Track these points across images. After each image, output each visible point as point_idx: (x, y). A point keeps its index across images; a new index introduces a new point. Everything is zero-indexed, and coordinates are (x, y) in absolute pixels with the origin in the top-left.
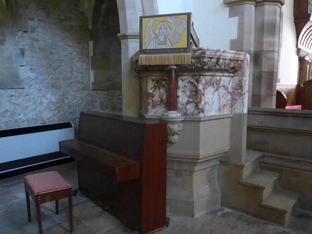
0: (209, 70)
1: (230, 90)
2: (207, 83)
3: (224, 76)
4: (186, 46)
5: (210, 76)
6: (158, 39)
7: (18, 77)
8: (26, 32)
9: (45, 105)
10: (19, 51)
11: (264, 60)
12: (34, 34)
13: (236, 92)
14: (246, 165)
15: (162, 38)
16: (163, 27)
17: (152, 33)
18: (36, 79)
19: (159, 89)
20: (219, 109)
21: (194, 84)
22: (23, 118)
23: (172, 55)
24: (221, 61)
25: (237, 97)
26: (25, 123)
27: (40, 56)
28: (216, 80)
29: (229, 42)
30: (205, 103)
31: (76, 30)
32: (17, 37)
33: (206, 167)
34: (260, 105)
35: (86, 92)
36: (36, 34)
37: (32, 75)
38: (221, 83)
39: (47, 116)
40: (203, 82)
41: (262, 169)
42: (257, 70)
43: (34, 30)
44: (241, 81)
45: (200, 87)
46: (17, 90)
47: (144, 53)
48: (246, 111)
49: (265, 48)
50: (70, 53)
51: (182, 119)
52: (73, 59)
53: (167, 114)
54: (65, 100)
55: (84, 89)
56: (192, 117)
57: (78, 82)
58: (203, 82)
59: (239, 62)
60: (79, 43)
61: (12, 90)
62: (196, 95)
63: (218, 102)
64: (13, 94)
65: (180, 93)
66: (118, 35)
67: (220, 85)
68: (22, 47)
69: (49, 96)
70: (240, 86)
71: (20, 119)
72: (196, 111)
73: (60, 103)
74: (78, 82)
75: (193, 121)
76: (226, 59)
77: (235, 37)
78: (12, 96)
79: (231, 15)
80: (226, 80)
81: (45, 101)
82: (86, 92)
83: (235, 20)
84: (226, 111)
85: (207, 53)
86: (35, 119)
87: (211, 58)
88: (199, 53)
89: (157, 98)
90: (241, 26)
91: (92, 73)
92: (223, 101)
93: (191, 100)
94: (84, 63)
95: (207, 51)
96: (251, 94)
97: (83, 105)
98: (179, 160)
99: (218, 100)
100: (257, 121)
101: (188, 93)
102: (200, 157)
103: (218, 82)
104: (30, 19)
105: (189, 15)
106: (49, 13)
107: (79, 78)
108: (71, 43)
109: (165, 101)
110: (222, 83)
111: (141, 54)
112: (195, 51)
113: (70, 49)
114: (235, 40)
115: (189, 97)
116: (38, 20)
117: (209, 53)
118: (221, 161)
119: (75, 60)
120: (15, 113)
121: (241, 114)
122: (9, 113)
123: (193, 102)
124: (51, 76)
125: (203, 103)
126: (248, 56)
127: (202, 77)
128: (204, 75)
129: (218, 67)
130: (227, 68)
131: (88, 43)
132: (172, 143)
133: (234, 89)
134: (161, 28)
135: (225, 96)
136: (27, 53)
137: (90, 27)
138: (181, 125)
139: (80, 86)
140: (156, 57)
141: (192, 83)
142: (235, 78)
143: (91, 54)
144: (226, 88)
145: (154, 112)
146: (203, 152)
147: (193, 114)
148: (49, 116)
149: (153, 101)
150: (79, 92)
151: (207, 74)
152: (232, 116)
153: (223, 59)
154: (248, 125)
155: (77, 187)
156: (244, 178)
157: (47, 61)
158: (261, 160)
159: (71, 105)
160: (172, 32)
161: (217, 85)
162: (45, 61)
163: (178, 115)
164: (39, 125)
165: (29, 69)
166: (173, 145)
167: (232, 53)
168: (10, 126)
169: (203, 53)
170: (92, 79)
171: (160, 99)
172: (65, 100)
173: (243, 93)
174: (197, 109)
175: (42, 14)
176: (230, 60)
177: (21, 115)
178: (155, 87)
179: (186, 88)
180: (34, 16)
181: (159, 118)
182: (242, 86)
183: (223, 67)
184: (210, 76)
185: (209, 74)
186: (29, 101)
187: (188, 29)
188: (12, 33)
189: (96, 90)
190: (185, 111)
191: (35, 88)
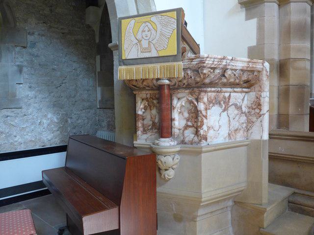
0: (212, 84)
1: (244, 109)
2: (210, 102)
3: (235, 92)
4: (176, 53)
5: (214, 92)
6: (141, 45)
7: (14, 95)
8: (24, 47)
9: (45, 125)
10: (15, 68)
11: (291, 70)
12: (34, 50)
13: (253, 112)
14: (268, 209)
15: (145, 44)
16: (146, 29)
17: (133, 38)
18: (36, 98)
19: (151, 110)
20: (229, 134)
21: (193, 103)
22: (20, 140)
23: (158, 66)
24: (229, 72)
25: (254, 119)
26: (22, 146)
27: (40, 73)
28: (224, 98)
29: (247, 49)
30: (209, 128)
31: (81, 44)
32: (14, 53)
33: (214, 209)
34: (287, 127)
35: (93, 111)
36: (37, 49)
37: (31, 94)
38: (231, 101)
39: (48, 137)
40: (205, 100)
41: (292, 210)
42: (283, 83)
43: (34, 45)
44: (258, 98)
45: (201, 106)
46: (13, 110)
47: (125, 64)
48: (266, 137)
49: (292, 56)
50: (74, 69)
51: (178, 149)
52: (78, 76)
53: (158, 142)
54: (69, 120)
55: (90, 108)
56: (191, 146)
57: (83, 100)
58: (205, 100)
59: (256, 73)
60: (86, 58)
61: (9, 110)
62: (195, 118)
63: (227, 125)
64: (9, 114)
65: (175, 115)
66: (110, 45)
67: (230, 104)
68: (20, 64)
69: (50, 116)
70: (258, 105)
71: (16, 141)
72: (196, 139)
73: (63, 123)
74: (83, 100)
75: (192, 150)
76: (236, 70)
77: (253, 43)
78: (7, 117)
79: (248, 18)
80: (238, 97)
81: (45, 121)
82: (93, 111)
83: (254, 22)
84: (240, 137)
85: (207, 62)
86: (33, 141)
87: (214, 69)
88: (196, 62)
89: (148, 122)
90: (260, 29)
91: (99, 89)
92: (235, 124)
93: (190, 124)
94: (91, 79)
95: (208, 59)
96: (275, 113)
97: (89, 125)
98: (262, 149)
99: (228, 123)
100: (284, 148)
101: (186, 115)
102: (203, 200)
103: (227, 99)
104: (29, 33)
105: (180, 12)
106: (51, 27)
107: (85, 96)
108: (75, 59)
109: (158, 124)
110: (232, 101)
111: (120, 65)
112: (192, 60)
113: (75, 65)
114: (254, 46)
115: (188, 120)
116: (39, 35)
117: (211, 62)
118: (235, 202)
119: (81, 76)
120: (11, 135)
121: (260, 141)
122: (4, 135)
123: (193, 126)
124: (52, 94)
125: (205, 127)
126: (267, 65)
127: (203, 94)
128: (206, 92)
129: (224, 80)
130: (237, 81)
131: (95, 58)
132: (166, 181)
133: (249, 108)
134: (143, 31)
135: (237, 118)
136: (25, 69)
137: (97, 41)
138: (177, 156)
139: (87, 104)
140: (138, 69)
141: (191, 102)
142: (251, 93)
143: (98, 69)
144: (239, 108)
145: (143, 140)
146: (208, 193)
147: (192, 143)
148: (49, 137)
149: (143, 125)
150: (84, 111)
151: (209, 89)
152: (247, 143)
153: (232, 70)
154: (269, 153)
155: (65, 224)
156: (265, 225)
157: (49, 78)
158: (291, 199)
159: (75, 124)
160: (158, 35)
161: (226, 104)
162: (46, 78)
163: (172, 143)
164: (37, 147)
165: (27, 87)
166: (169, 182)
167: (245, 62)
168: (5, 150)
169: (202, 62)
170: (99, 97)
171: (151, 123)
172: (69, 120)
173: (261, 113)
174: (198, 136)
175: (43, 29)
176: (242, 70)
177: (18, 137)
178: (145, 108)
179: (183, 109)
180: (35, 31)
181: (149, 146)
182: (259, 105)
183: (232, 80)
184: (214, 92)
185: (213, 89)
186: (27, 121)
187: (177, 29)
188: (8, 49)
189: (103, 108)
190: (182, 138)
191: (34, 107)
